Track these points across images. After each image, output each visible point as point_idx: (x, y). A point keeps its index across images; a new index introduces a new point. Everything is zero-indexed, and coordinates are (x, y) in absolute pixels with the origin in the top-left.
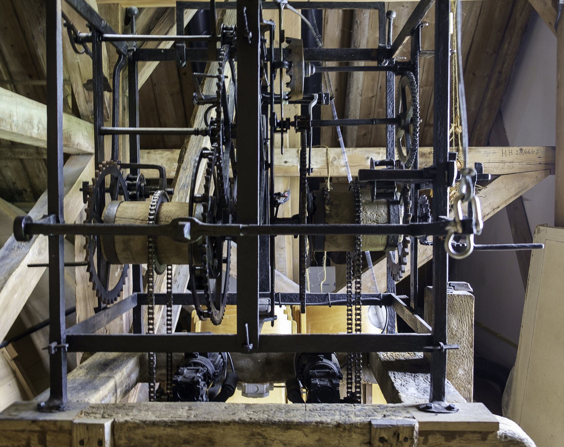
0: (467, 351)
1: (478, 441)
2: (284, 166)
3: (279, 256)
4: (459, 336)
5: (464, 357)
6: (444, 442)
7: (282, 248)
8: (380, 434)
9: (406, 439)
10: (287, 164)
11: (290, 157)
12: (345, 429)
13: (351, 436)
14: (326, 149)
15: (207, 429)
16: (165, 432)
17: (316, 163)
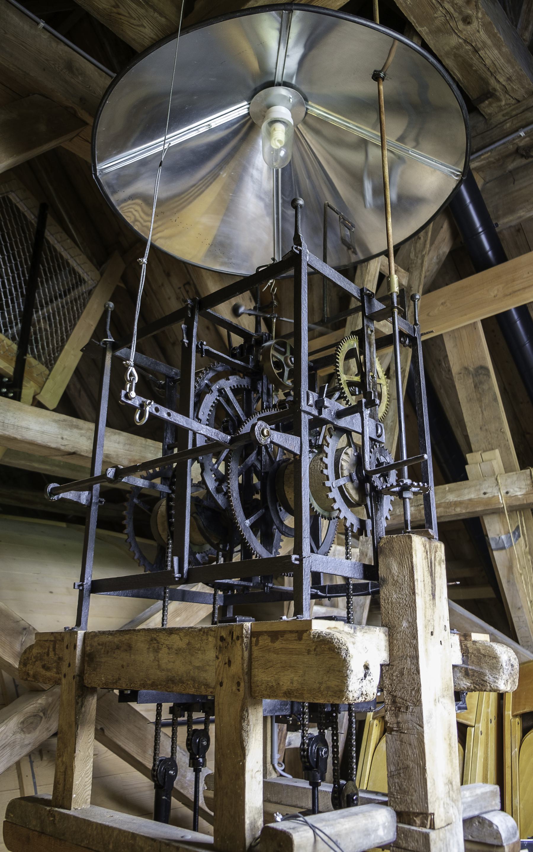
0: (409, 599)
1: (295, 642)
2: (484, 498)
3: (517, 618)
4: (400, 581)
5: (407, 606)
6: (270, 644)
7: (519, 608)
8: (220, 633)
9: (238, 638)
10: (487, 496)
11: (489, 486)
12: (204, 632)
13: (207, 639)
14: (529, 470)
15: (128, 636)
16: (107, 639)
17: (520, 488)
